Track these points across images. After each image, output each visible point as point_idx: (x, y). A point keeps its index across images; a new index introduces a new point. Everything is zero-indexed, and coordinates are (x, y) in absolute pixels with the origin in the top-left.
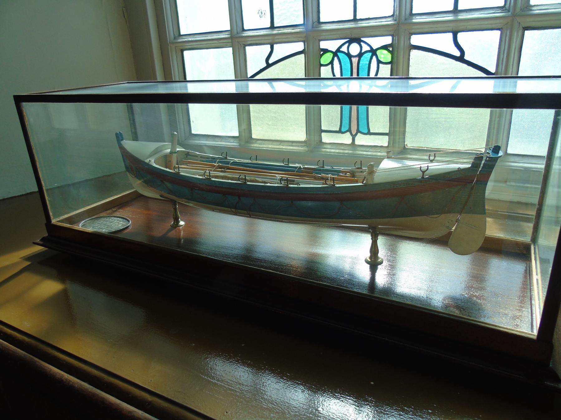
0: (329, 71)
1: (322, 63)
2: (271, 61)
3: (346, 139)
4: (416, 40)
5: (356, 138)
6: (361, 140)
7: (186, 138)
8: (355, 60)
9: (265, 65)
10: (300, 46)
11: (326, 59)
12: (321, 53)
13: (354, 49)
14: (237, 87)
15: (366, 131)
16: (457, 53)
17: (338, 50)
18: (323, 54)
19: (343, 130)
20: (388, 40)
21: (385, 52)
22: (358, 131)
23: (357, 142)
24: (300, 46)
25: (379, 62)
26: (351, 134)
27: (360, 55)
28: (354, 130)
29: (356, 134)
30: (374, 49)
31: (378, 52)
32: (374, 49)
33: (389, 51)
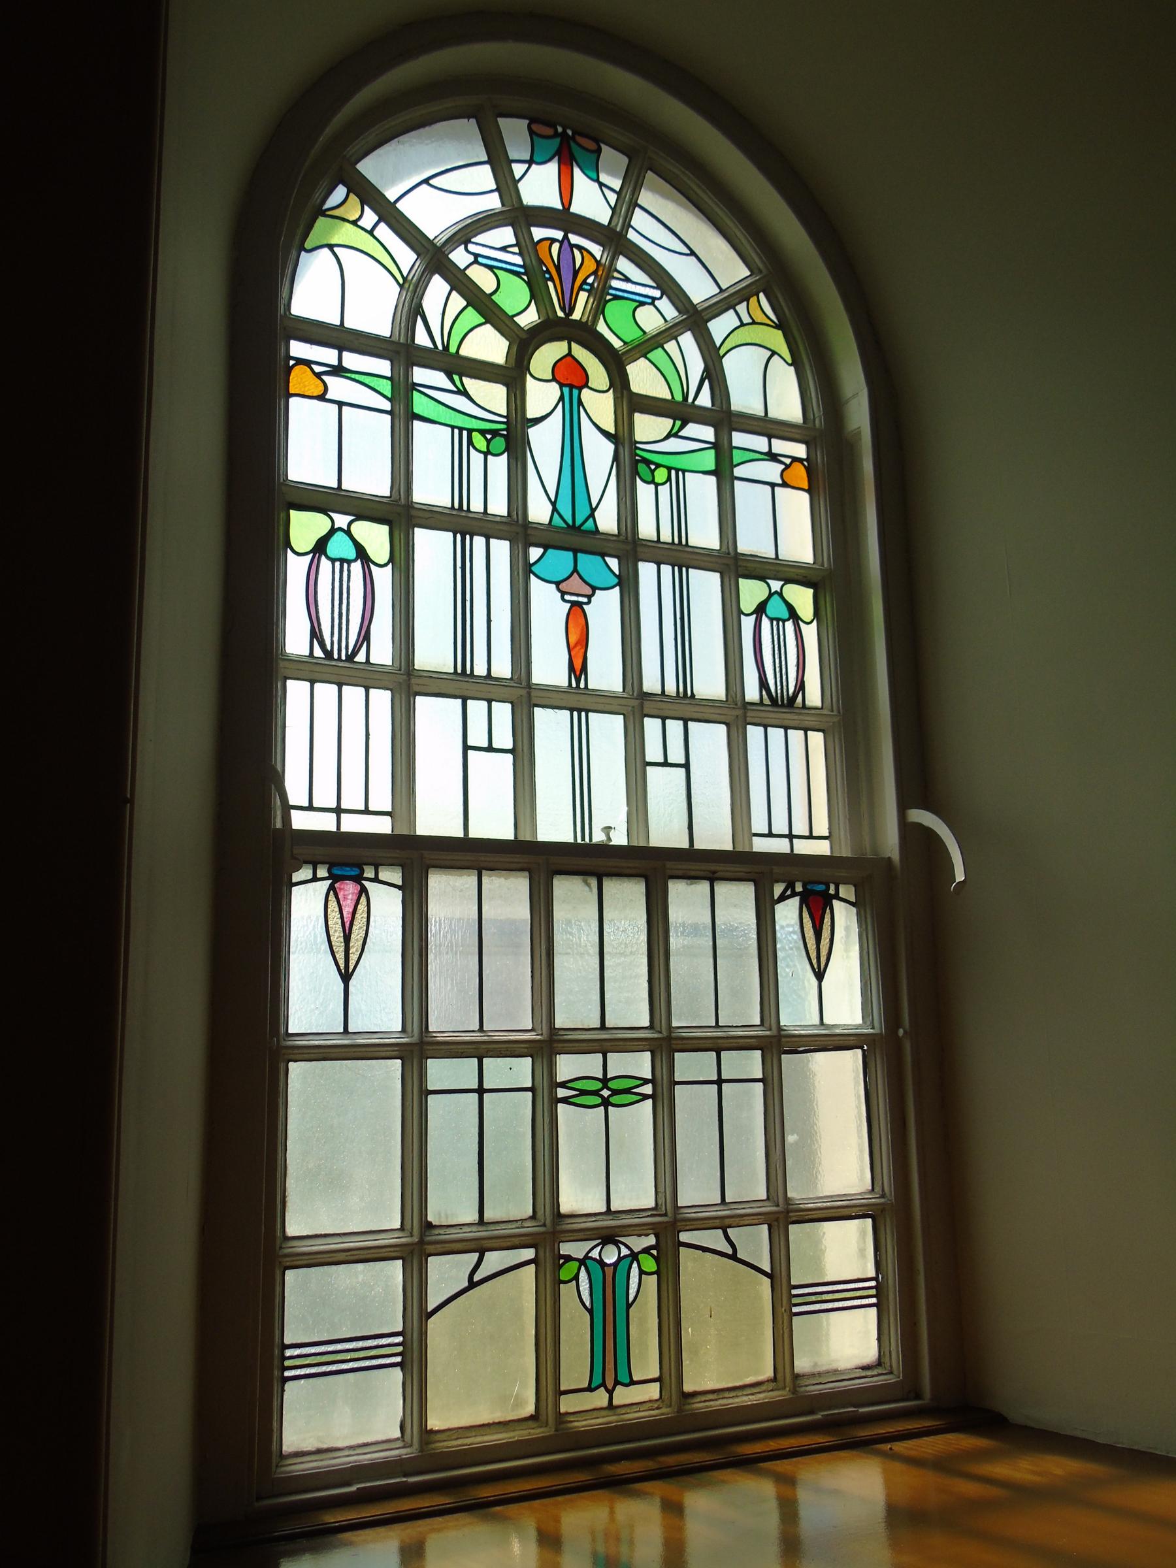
0: (432, 1143)
1: (562, 1278)
2: (476, 1278)
4: (684, 1237)
11: (565, 1274)
12: (561, 1262)
13: (610, 1255)
15: (627, 1381)
16: (730, 1251)
17: (587, 1257)
18: (564, 1264)
20: (651, 1240)
22: (617, 1383)
23: (615, 1402)
24: (529, 1254)
25: (642, 1273)
26: (607, 1390)
27: (620, 1259)
29: (614, 1388)
30: (342, 807)
32: (342, 807)
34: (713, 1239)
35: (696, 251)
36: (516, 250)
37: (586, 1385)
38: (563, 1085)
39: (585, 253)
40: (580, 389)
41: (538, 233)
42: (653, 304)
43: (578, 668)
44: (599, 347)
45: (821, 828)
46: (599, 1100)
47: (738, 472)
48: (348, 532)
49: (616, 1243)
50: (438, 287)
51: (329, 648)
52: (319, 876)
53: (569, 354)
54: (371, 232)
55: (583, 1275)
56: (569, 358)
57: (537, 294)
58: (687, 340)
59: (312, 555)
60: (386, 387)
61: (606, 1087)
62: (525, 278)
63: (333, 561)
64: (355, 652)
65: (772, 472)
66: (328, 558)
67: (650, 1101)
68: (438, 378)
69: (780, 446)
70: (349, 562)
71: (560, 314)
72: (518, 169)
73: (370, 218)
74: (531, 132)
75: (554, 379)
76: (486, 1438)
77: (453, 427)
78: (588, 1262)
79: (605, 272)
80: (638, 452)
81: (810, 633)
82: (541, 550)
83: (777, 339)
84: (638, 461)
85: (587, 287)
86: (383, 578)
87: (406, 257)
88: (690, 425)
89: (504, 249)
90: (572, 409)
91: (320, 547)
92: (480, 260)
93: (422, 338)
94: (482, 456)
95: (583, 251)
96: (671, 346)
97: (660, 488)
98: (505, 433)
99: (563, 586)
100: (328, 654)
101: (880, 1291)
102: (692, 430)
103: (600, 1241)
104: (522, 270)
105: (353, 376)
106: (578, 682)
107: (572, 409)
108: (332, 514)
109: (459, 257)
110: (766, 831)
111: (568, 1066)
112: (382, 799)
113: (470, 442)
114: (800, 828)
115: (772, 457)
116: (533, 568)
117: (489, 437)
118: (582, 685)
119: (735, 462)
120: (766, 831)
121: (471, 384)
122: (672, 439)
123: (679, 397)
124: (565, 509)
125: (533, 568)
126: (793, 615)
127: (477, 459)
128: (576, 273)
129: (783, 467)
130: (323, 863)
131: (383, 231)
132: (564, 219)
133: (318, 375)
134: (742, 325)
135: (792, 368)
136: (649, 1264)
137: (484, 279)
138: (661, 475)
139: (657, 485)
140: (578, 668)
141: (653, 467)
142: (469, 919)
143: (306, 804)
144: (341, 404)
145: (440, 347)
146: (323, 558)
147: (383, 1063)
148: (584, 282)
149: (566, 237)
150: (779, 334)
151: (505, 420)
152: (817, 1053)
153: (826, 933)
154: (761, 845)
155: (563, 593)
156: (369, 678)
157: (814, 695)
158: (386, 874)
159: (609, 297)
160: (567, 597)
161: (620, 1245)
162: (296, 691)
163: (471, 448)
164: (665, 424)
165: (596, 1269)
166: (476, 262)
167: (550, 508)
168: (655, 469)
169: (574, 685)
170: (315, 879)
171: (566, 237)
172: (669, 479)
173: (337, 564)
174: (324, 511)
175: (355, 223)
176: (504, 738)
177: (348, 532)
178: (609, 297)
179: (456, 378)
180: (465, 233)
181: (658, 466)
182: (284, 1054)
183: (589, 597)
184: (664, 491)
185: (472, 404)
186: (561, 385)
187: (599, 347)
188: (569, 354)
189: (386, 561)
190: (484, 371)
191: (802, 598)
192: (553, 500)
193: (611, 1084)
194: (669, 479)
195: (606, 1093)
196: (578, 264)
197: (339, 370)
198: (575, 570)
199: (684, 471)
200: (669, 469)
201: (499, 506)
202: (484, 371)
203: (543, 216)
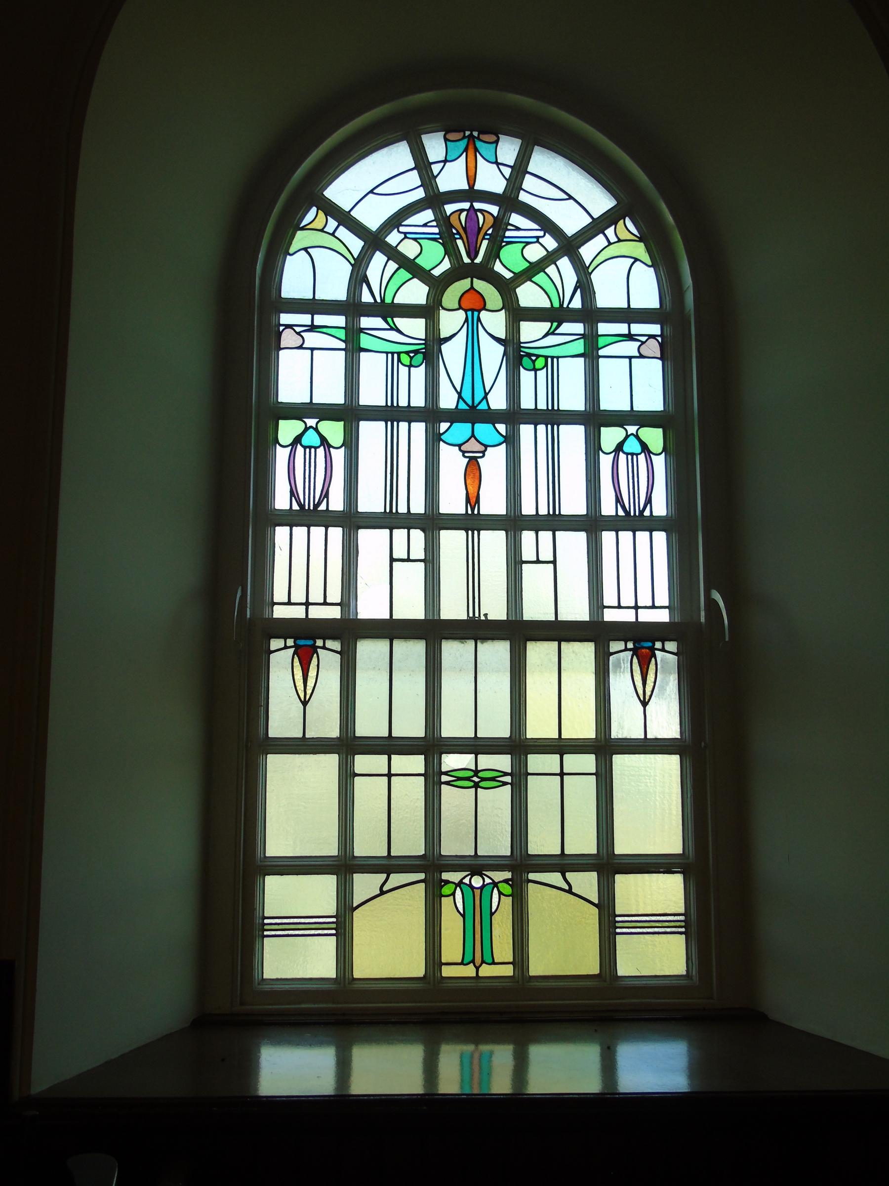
2: (385, 889)
3: (469, 971)
5: (480, 969)
6: (486, 971)
7: (665, 681)
8: (478, 892)
9: (379, 892)
10: (422, 876)
11: (446, 890)
13: (477, 882)
14: (667, 672)
15: (490, 961)
16: (567, 888)
17: (461, 882)
18: (444, 885)
19: (465, 962)
20: (508, 875)
21: (505, 885)
22: (483, 962)
24: (422, 876)
25: (500, 893)
26: (475, 965)
27: (484, 886)
28: (478, 960)
29: (480, 966)
31: (500, 885)
33: (509, 884)
34: (555, 878)
35: (370, 190)
36: (434, 223)
37: (460, 961)
38: (446, 773)
39: (486, 214)
40: (479, 311)
41: (450, 208)
42: (538, 242)
43: (473, 500)
44: (495, 280)
45: (663, 598)
46: (472, 784)
47: (601, 352)
48: (316, 429)
49: (481, 875)
50: (379, 258)
51: (628, 510)
52: (288, 645)
53: (472, 288)
54: (333, 234)
55: (458, 892)
56: (472, 291)
57: (451, 251)
58: (565, 263)
59: (291, 447)
60: (342, 334)
61: (476, 775)
62: (441, 241)
63: (627, 454)
64: (319, 503)
65: (631, 348)
66: (624, 453)
67: (509, 786)
68: (378, 322)
69: (637, 328)
70: (637, 455)
71: (466, 260)
72: (436, 169)
73: (332, 224)
74: (446, 140)
75: (460, 308)
76: (581, 983)
77: (387, 353)
78: (462, 886)
79: (500, 224)
80: (522, 349)
81: (659, 462)
82: (448, 424)
83: (640, 250)
84: (524, 356)
85: (488, 237)
86: (339, 456)
87: (356, 245)
88: (565, 325)
89: (425, 225)
90: (473, 326)
91: (619, 448)
92: (408, 236)
93: (366, 297)
94: (407, 368)
95: (483, 212)
96: (551, 270)
97: (538, 372)
98: (424, 350)
99: (463, 448)
100: (302, 506)
101: (687, 924)
102: (566, 327)
103: (469, 872)
104: (438, 236)
105: (324, 330)
106: (473, 510)
107: (473, 326)
108: (305, 420)
109: (393, 238)
110: (286, 600)
111: (452, 761)
112: (335, 595)
113: (399, 360)
114: (645, 599)
115: (630, 337)
116: (442, 437)
117: (412, 355)
118: (476, 512)
119: (600, 345)
120: (650, 604)
121: (400, 322)
122: (550, 337)
123: (556, 304)
124: (467, 396)
125: (442, 437)
126: (645, 448)
127: (404, 370)
128: (480, 229)
129: (640, 343)
130: (630, 640)
131: (343, 232)
132: (471, 194)
133: (299, 334)
134: (610, 244)
135: (652, 269)
136: (506, 889)
137: (409, 249)
138: (540, 363)
139: (535, 370)
140: (473, 500)
141: (534, 358)
142: (620, 672)
143: (616, 605)
144: (312, 349)
145: (379, 300)
146: (621, 453)
147: (626, 759)
148: (486, 234)
149: (472, 206)
150: (641, 246)
151: (424, 342)
152: (451, 755)
153: (312, 673)
154: (610, 616)
155: (464, 452)
156: (328, 520)
157: (660, 508)
158: (330, 644)
159: (504, 244)
160: (466, 455)
161: (484, 877)
162: (281, 533)
163: (399, 363)
164: (545, 326)
165: (467, 890)
166: (406, 237)
167: (457, 396)
168: (536, 360)
169: (470, 512)
170: (286, 647)
171: (472, 206)
172: (546, 365)
173: (630, 457)
174: (300, 419)
175: (322, 230)
176: (418, 551)
177: (316, 429)
178: (504, 244)
179: (389, 320)
180: (395, 221)
181: (538, 356)
182: (342, 749)
183: (483, 452)
184: (542, 374)
185: (402, 336)
186: (466, 311)
187: (495, 280)
188: (472, 288)
189: (660, 451)
190: (536, 315)
191: (654, 437)
192: (459, 391)
193: (480, 774)
194: (546, 365)
195: (476, 779)
196: (481, 223)
197: (312, 328)
198: (473, 435)
199: (558, 358)
200: (546, 357)
201: (418, 401)
202: (536, 315)
203: (455, 196)
